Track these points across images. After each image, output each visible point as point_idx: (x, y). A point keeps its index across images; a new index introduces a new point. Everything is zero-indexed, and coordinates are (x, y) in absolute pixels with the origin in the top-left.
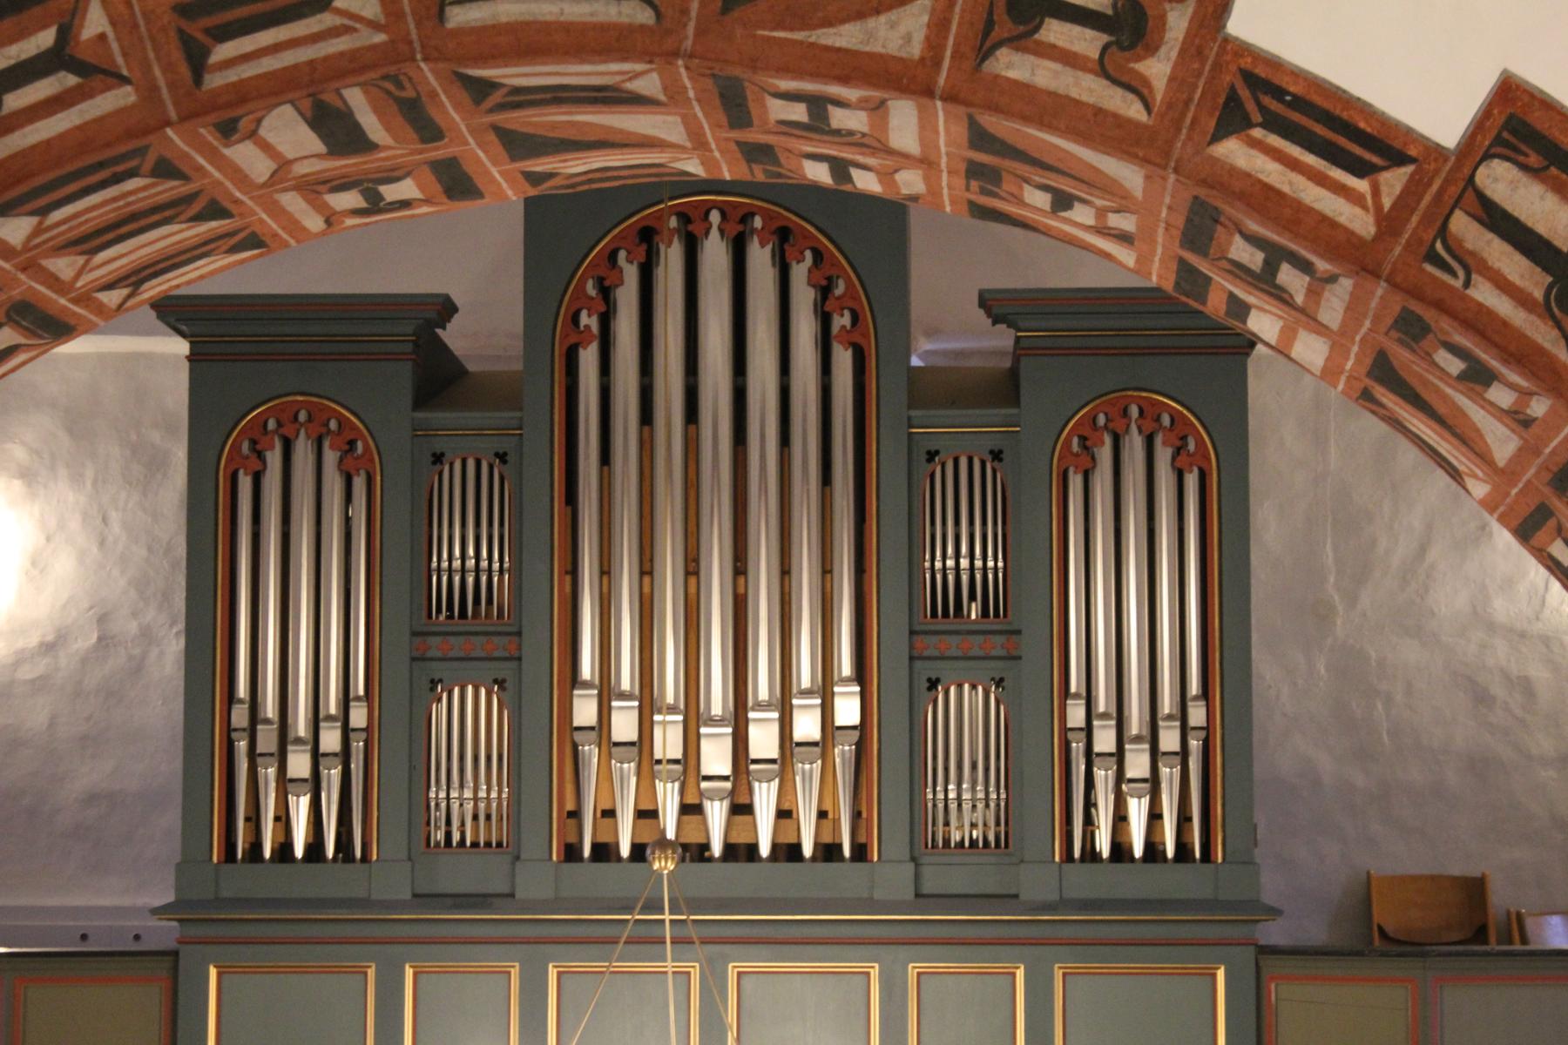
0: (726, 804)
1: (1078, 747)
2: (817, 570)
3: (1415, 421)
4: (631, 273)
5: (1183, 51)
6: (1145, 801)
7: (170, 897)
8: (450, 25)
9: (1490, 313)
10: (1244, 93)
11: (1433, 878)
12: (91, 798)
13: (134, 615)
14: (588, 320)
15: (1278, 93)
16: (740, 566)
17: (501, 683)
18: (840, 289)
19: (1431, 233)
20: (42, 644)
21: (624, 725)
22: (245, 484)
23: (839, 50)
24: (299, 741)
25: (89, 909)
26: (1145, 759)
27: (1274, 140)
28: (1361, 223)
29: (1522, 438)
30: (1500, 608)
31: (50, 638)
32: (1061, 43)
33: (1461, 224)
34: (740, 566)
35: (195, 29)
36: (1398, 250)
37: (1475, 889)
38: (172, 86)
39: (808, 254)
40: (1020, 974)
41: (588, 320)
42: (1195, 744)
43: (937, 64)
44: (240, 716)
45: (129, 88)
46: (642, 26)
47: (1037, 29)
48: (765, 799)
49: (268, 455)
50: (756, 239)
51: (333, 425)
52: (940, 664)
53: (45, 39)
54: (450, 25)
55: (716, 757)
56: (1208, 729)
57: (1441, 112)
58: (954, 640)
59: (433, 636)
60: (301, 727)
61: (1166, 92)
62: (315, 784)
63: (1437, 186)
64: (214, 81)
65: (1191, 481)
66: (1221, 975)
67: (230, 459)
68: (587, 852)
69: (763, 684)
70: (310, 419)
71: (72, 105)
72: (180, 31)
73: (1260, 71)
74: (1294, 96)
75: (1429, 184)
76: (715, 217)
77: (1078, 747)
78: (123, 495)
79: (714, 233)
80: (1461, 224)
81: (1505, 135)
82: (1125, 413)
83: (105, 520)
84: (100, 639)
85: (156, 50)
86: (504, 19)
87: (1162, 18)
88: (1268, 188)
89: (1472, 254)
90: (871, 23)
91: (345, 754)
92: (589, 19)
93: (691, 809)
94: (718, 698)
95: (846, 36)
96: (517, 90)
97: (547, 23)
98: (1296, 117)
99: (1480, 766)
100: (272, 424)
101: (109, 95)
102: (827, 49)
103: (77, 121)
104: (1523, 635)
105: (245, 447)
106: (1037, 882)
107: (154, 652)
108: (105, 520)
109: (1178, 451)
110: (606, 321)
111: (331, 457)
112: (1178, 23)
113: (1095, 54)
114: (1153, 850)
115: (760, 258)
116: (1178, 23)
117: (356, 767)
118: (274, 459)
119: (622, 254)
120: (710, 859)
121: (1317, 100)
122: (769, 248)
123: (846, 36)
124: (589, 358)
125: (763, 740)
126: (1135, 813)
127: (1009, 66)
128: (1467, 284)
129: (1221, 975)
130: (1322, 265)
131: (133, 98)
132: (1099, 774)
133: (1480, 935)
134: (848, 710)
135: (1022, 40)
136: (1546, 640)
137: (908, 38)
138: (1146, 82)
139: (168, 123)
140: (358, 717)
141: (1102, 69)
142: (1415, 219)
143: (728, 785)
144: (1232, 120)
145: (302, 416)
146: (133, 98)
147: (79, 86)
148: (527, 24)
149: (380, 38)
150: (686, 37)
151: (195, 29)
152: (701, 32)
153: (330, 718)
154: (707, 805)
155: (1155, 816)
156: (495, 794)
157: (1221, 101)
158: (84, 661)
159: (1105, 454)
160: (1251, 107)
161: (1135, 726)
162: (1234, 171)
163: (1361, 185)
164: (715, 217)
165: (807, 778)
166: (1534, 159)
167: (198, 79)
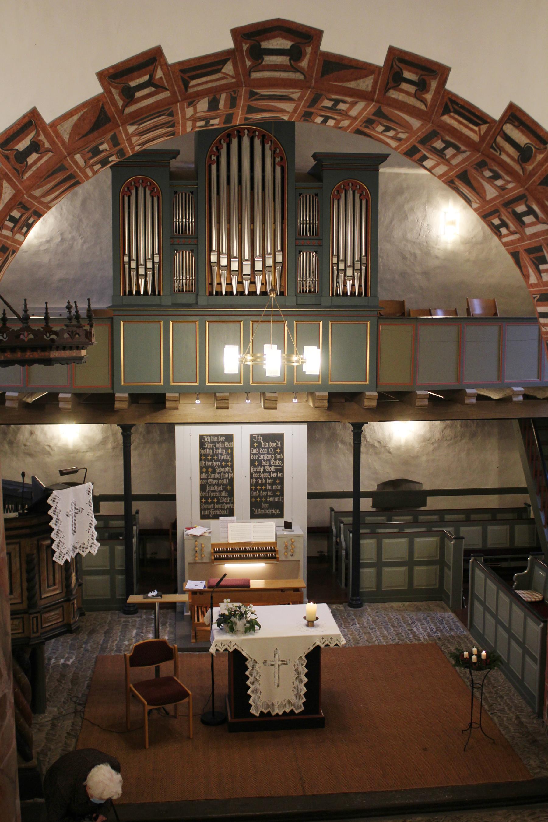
0: (249, 281)
1: (335, 268)
2: (261, 223)
3: (464, 189)
4: (225, 146)
5: (435, 93)
6: (351, 282)
7: (111, 305)
8: (252, 77)
9: (505, 162)
10: (449, 104)
11: (391, 301)
12: (61, 280)
13: (70, 233)
14: (213, 158)
15: (457, 104)
16: (252, 222)
17: (192, 251)
18: (278, 151)
19: (492, 141)
20: (46, 241)
21: (224, 262)
22: (126, 198)
23: (350, 88)
24: (141, 265)
25: (55, 308)
26: (351, 271)
27: (456, 116)
28: (475, 137)
29: (499, 192)
30: (410, 236)
31: (48, 239)
32: (405, 89)
33: (499, 140)
34: (252, 222)
35: (186, 76)
36: (484, 145)
37: (402, 304)
38: (179, 92)
39: (270, 142)
40: (321, 323)
41: (213, 158)
42: (363, 268)
43: (375, 92)
44: (126, 259)
45: (168, 92)
46: (301, 80)
47: (400, 85)
48: (259, 280)
49: (132, 191)
50: (257, 138)
51: (149, 184)
52: (302, 247)
53: (146, 78)
54: (252, 77)
55: (247, 270)
56: (159, 262)
57: (495, 111)
58: (305, 241)
59: (173, 241)
60: (142, 262)
61: (431, 102)
62: (146, 276)
63: (495, 128)
64: (191, 90)
65: (155, 199)
66: (369, 323)
67: (123, 192)
68: (214, 294)
69: (258, 252)
70: (143, 182)
71: (153, 96)
72: (182, 77)
73: (454, 98)
74: (461, 105)
75: (492, 129)
76: (246, 131)
77: (335, 268)
78: (66, 202)
79: (246, 136)
80: (499, 140)
81: (510, 117)
82: (348, 185)
83: (62, 208)
84: (61, 239)
85: (175, 81)
86: (266, 77)
87: (430, 84)
88: (454, 128)
89: (502, 147)
90: (359, 81)
91: (153, 269)
92: (287, 77)
93: (240, 283)
94: (247, 254)
95: (352, 85)
96: (262, 96)
97: (278, 78)
98: (461, 110)
99: (403, 274)
100: (133, 183)
101: (163, 93)
102: (347, 88)
103: (155, 100)
104: (414, 243)
105: (126, 189)
106: (326, 301)
107: (75, 243)
108: (62, 208)
109: (361, 195)
110: (218, 158)
111: (148, 192)
112: (434, 85)
113: (413, 92)
114: (353, 294)
115: (257, 143)
116: (434, 85)
117: (156, 271)
118: (133, 192)
119: (222, 141)
120: (245, 295)
121: (466, 106)
122: (260, 140)
123: (352, 85)
124: (214, 167)
125: (259, 266)
126: (348, 284)
127: (393, 94)
128: (500, 154)
129: (369, 323)
130: (463, 148)
131: (169, 95)
132: (340, 275)
133: (403, 314)
134: (279, 258)
135: (396, 88)
136: (420, 244)
137: (367, 86)
138: (426, 100)
139: (179, 101)
140: (157, 259)
141: (415, 96)
142: (488, 138)
143: (249, 277)
144: (446, 111)
145: (141, 181)
146: (169, 95)
147: (155, 91)
148: (272, 78)
149: (234, 80)
150: (312, 83)
151: (186, 76)
152: (316, 82)
153: (149, 259)
154: (244, 281)
155: (353, 285)
156: (192, 278)
157: (444, 105)
158: (57, 245)
159: (343, 195)
160: (451, 107)
161: (349, 263)
162: (447, 124)
163: (476, 128)
164: (246, 131)
165: (269, 275)
166: (516, 124)
167: (186, 90)
